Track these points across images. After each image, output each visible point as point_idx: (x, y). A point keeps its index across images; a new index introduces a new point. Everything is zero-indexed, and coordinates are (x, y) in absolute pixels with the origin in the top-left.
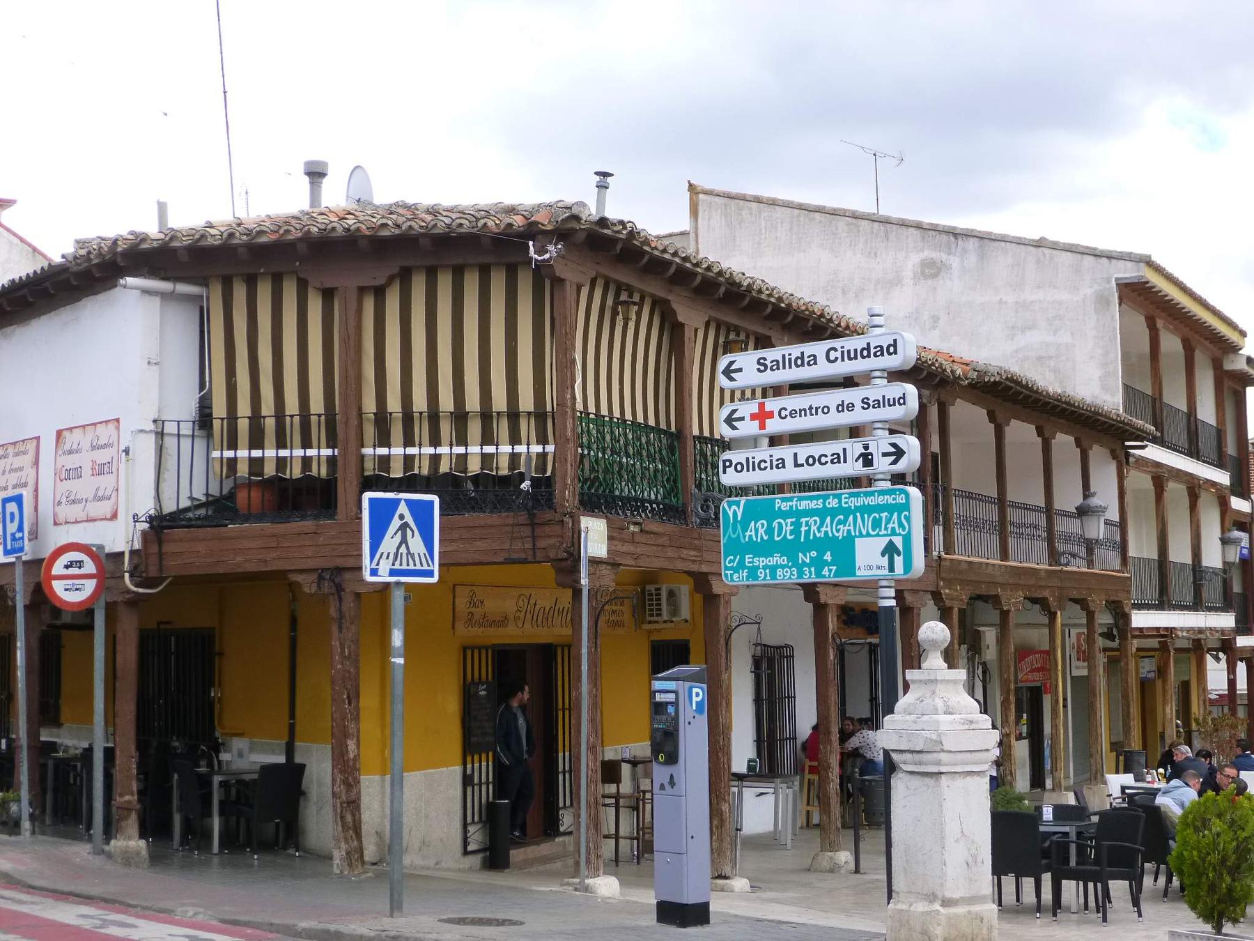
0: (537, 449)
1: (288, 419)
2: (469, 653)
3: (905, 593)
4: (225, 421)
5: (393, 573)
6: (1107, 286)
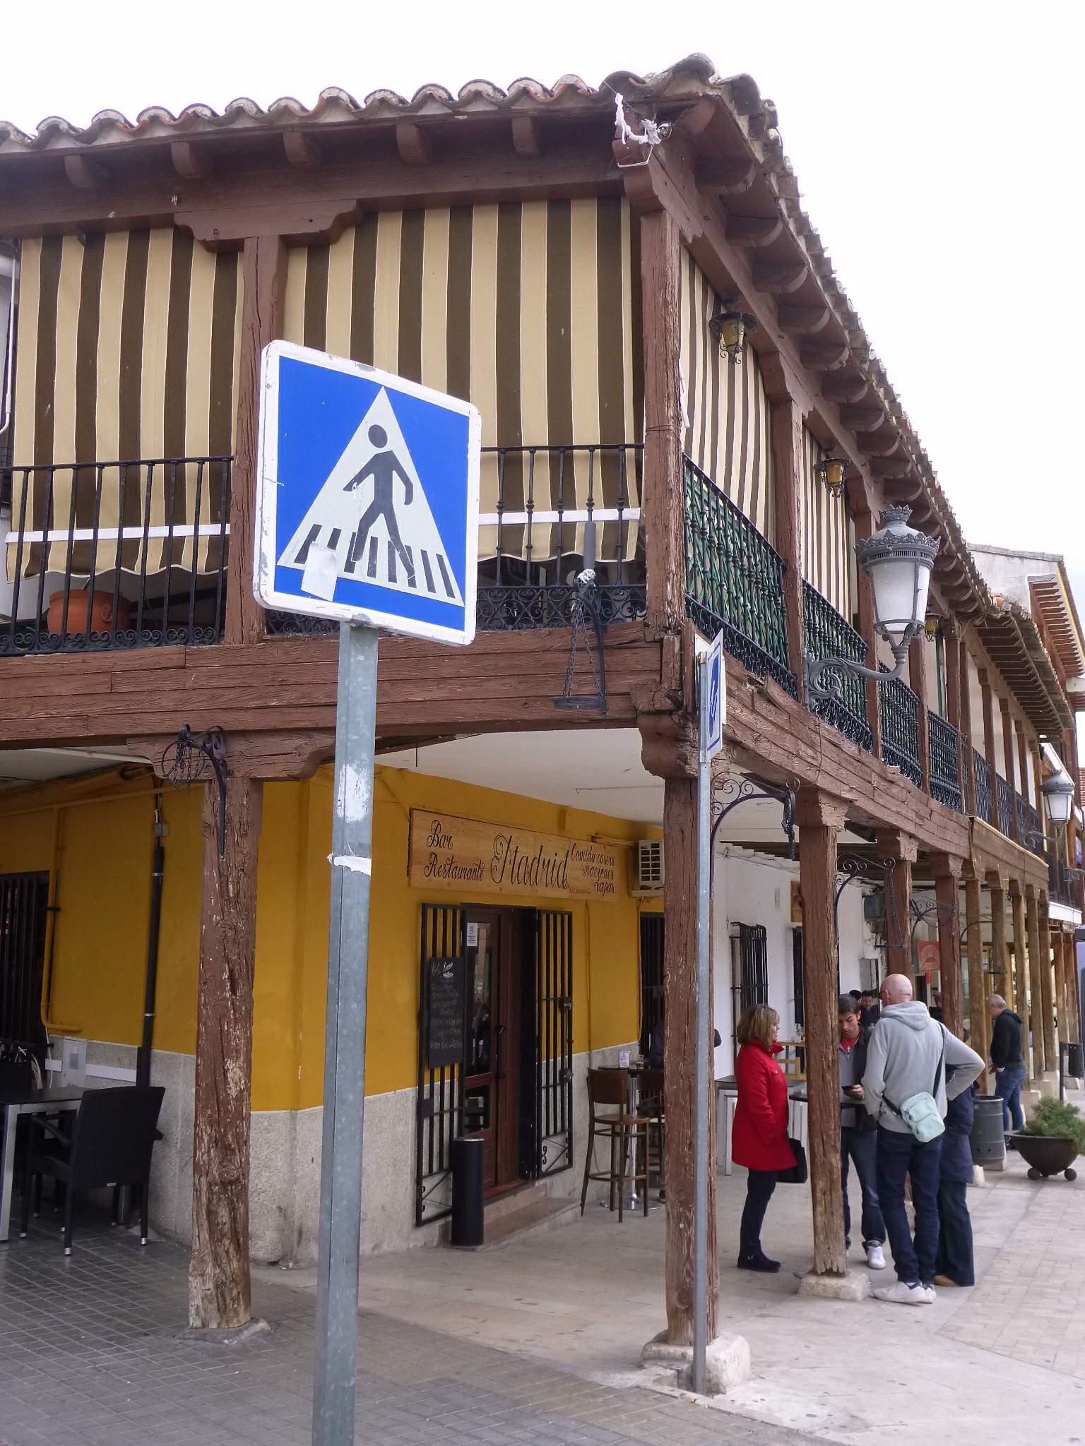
0: (606, 515)
1: (144, 469)
2: (430, 913)
3: (950, 856)
4: (32, 474)
5: (346, 591)
6: (1019, 585)
